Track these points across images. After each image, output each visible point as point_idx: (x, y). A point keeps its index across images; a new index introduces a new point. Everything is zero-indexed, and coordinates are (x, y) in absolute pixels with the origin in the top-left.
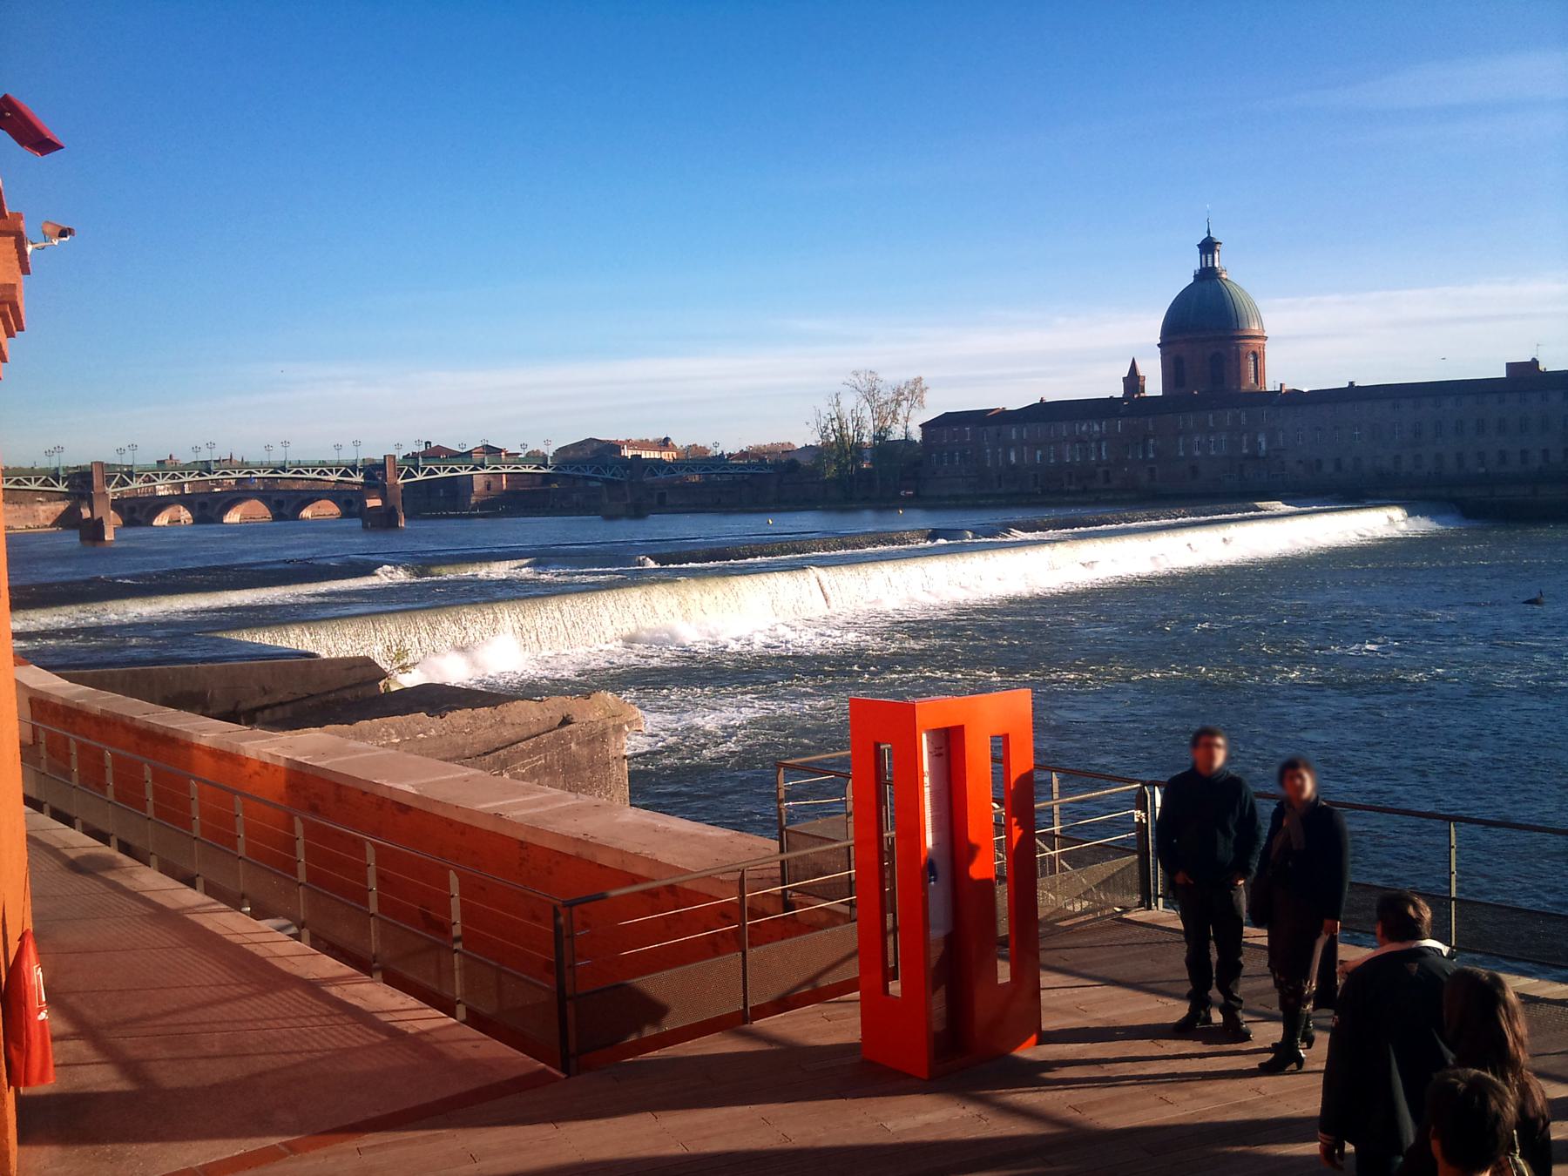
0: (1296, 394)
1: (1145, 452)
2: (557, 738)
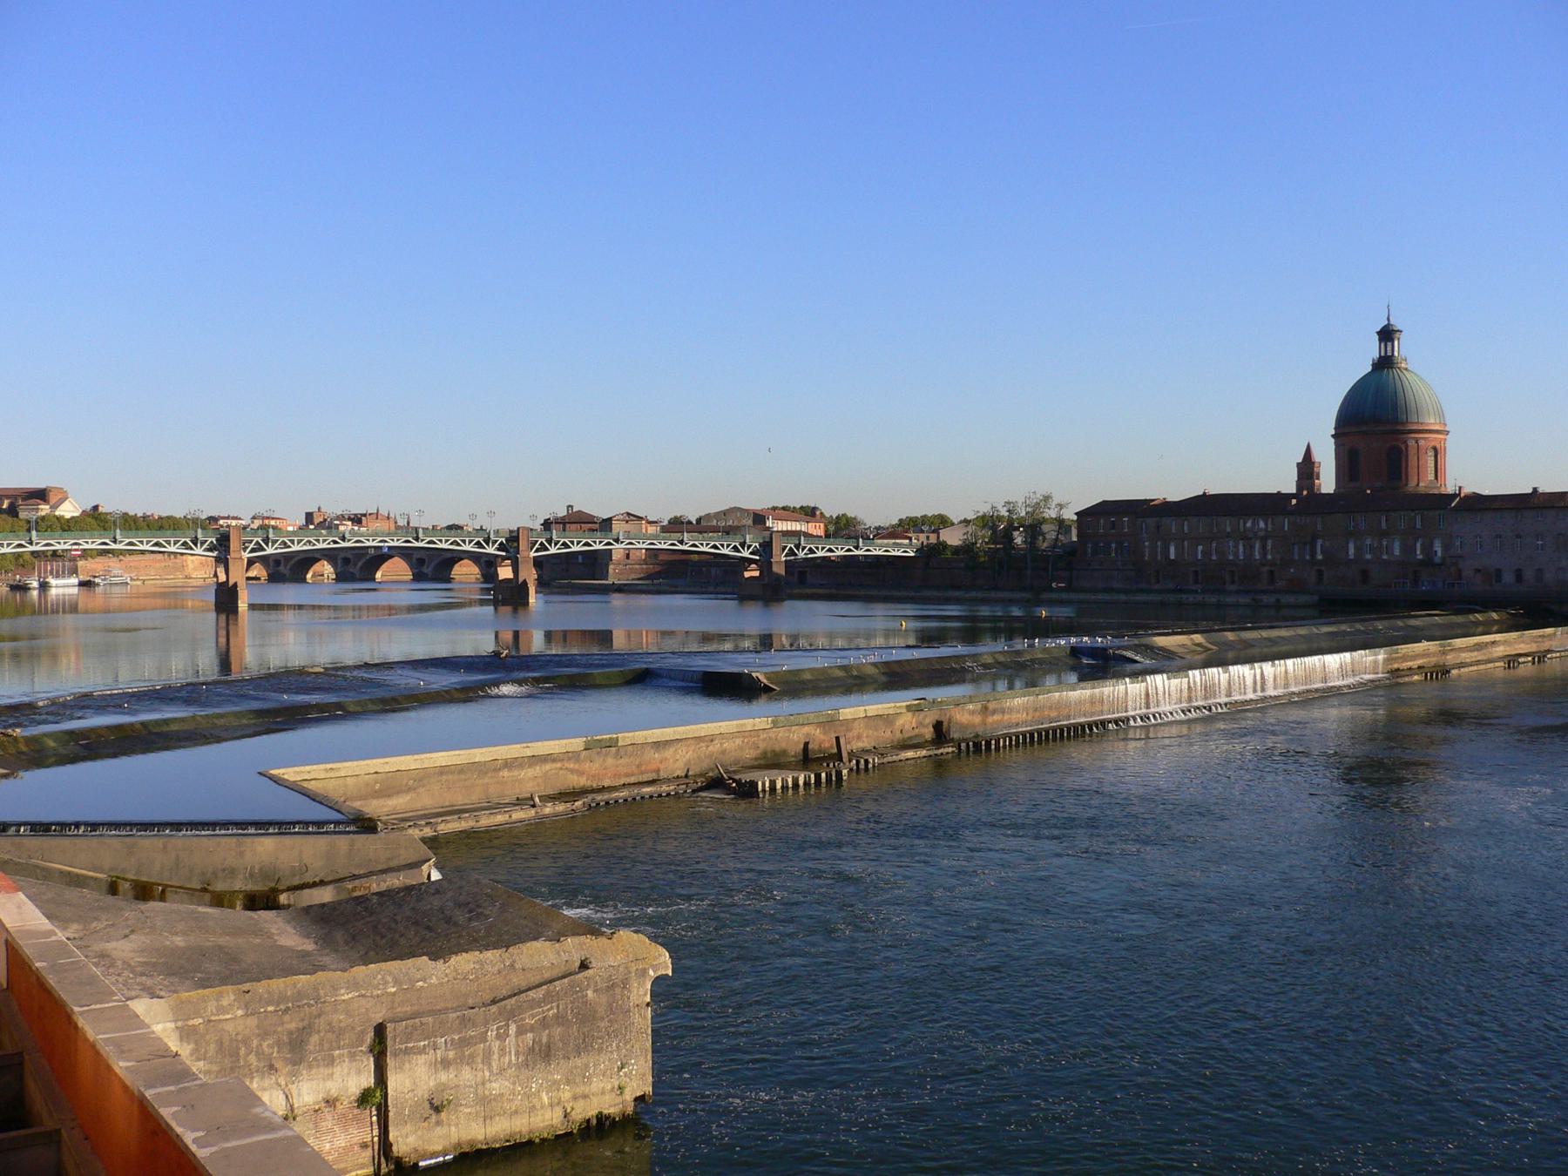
0: (1476, 498)
1: (1313, 554)
2: (572, 985)
